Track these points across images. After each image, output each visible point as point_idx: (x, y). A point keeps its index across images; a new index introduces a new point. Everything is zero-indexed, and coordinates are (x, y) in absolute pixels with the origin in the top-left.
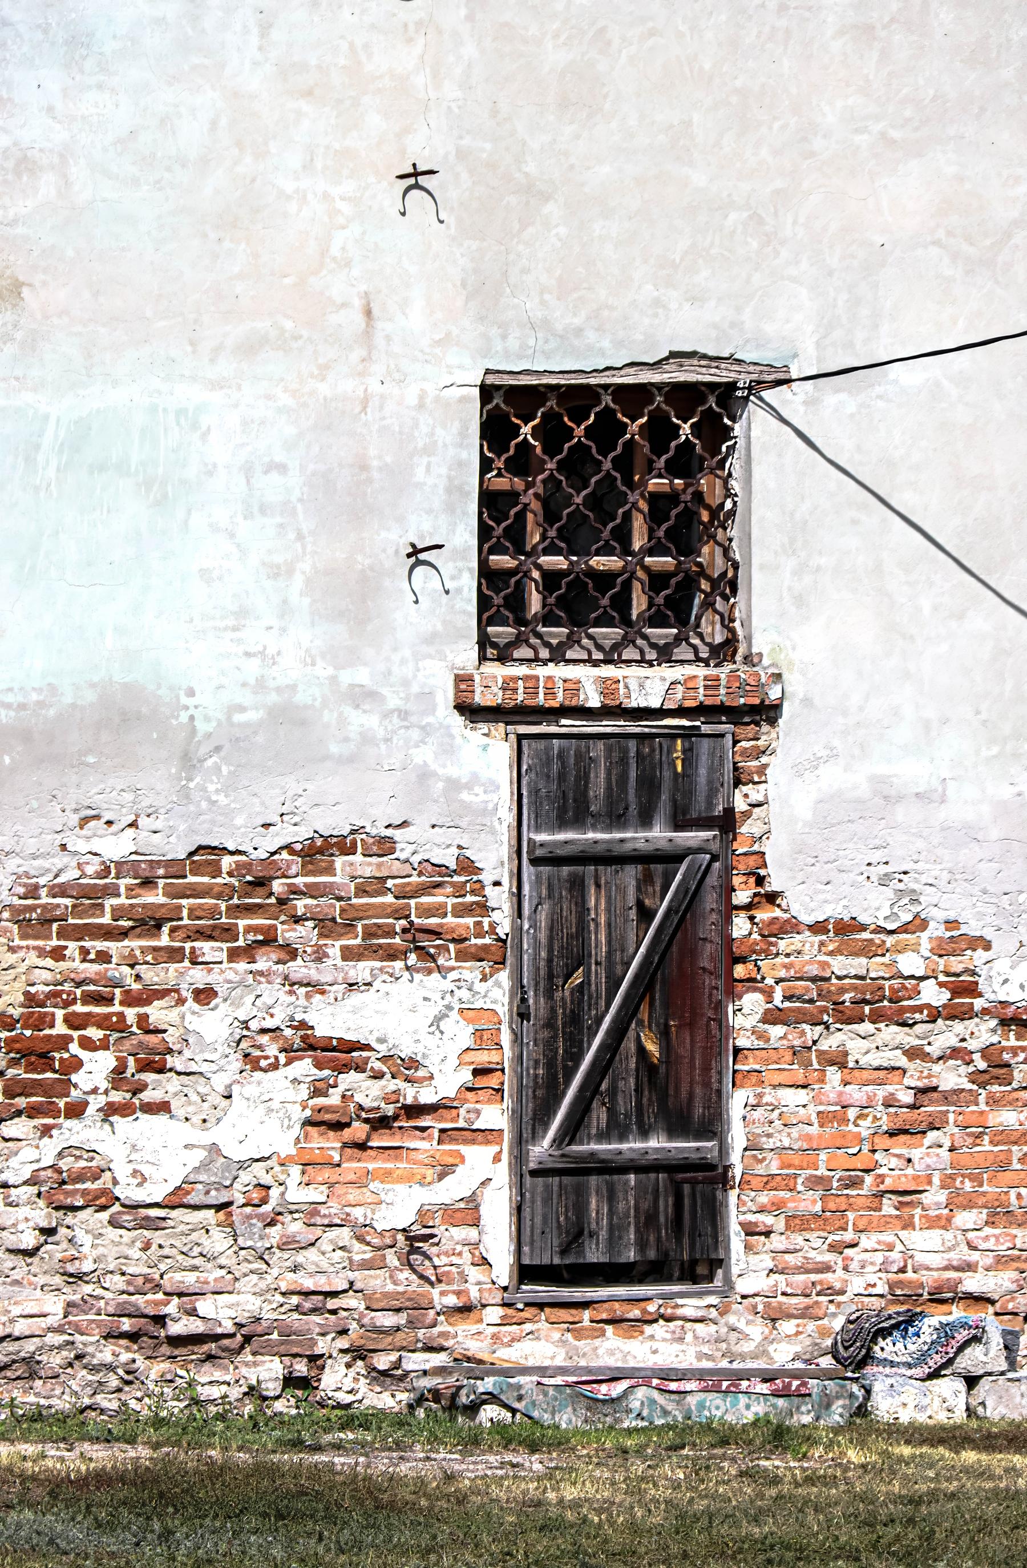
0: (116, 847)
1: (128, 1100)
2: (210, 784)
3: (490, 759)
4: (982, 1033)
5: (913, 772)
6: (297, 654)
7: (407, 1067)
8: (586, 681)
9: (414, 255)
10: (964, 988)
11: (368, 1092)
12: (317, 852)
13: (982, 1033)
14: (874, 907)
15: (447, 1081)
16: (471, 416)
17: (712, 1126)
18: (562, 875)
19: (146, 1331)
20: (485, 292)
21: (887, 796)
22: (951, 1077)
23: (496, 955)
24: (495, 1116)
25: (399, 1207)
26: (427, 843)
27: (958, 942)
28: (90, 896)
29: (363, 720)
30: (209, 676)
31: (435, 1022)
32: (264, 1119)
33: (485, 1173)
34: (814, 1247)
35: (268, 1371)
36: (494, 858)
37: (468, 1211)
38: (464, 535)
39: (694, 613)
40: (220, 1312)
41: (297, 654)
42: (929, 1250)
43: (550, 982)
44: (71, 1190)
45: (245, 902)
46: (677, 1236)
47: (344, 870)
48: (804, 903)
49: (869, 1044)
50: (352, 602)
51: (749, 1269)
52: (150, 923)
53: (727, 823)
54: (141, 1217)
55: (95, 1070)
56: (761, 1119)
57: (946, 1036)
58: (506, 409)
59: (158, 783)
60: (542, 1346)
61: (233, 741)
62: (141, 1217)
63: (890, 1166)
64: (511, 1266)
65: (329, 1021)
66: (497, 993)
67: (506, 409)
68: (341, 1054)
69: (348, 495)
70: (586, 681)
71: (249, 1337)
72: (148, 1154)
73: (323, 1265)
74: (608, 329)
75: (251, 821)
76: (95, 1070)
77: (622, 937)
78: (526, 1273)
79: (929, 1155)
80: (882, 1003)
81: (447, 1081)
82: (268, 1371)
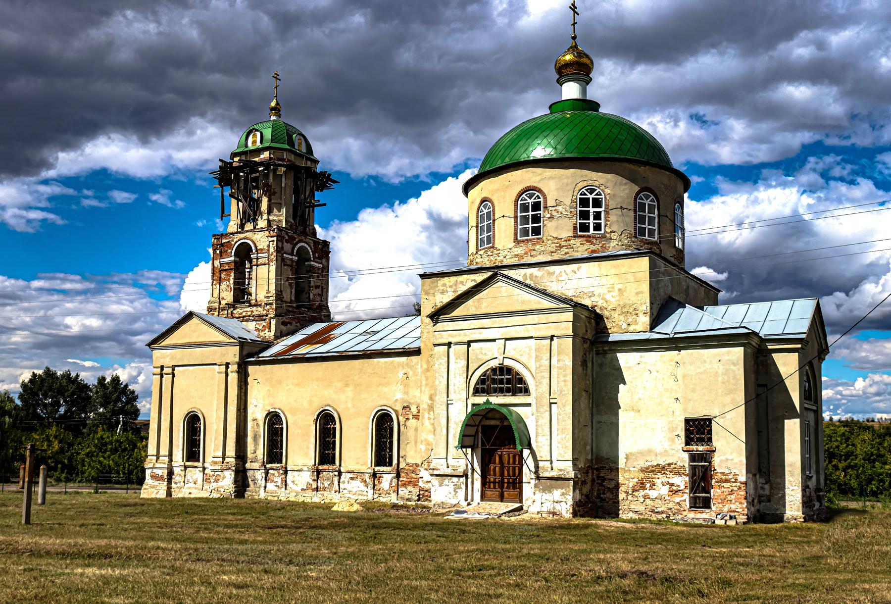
0: (650, 464)
1: (651, 488)
2: (658, 458)
3: (686, 456)
4: (738, 484)
5: (730, 457)
6: (667, 445)
7: (679, 486)
8: (695, 448)
9: (678, 407)
10: (736, 479)
11: (674, 488)
12: (669, 465)
13: (738, 484)
14: (727, 471)
15: (682, 487)
16: (682, 425)
17: (709, 492)
18: (693, 468)
19: (653, 511)
20: (685, 410)
21: (727, 460)
22: (735, 489)
23: (687, 475)
24: (687, 491)
25: (677, 500)
26: (680, 464)
27: (735, 475)
28: (647, 469)
29: (673, 452)
30: (659, 449)
31: (682, 482)
32: (665, 490)
33: (686, 497)
34: (721, 506)
35: (664, 516)
36: (687, 465)
37: (685, 501)
38: (683, 433)
39: (78, 361)
40: (660, 510)
41: (667, 445)
42: (733, 507)
43: (692, 478)
44: (646, 497)
45: (663, 469)
46: (706, 504)
47: (672, 466)
48: (719, 470)
49: (726, 485)
50: (672, 440)
51: (713, 508)
52: (653, 471)
53: (710, 462)
54: (653, 500)
55: (648, 485)
56: (715, 492)
57: (735, 484)
58: (687, 421)
59: (653, 458)
60: (691, 515)
61: (661, 454)
62: (653, 500)
63: (729, 498)
64: (620, 15)
65: (671, 481)
66: (687, 479)
67: (687, 421)
68: (672, 485)
69: (672, 430)
70: (695, 448)
71: (663, 512)
72: (653, 494)
73: (671, 505)
74: (698, 412)
75: (662, 461)
76: (648, 485)
77: (699, 473)
78: (691, 507)
79: (733, 497)
80: (727, 481)
81: (682, 487)
82: (664, 516)
